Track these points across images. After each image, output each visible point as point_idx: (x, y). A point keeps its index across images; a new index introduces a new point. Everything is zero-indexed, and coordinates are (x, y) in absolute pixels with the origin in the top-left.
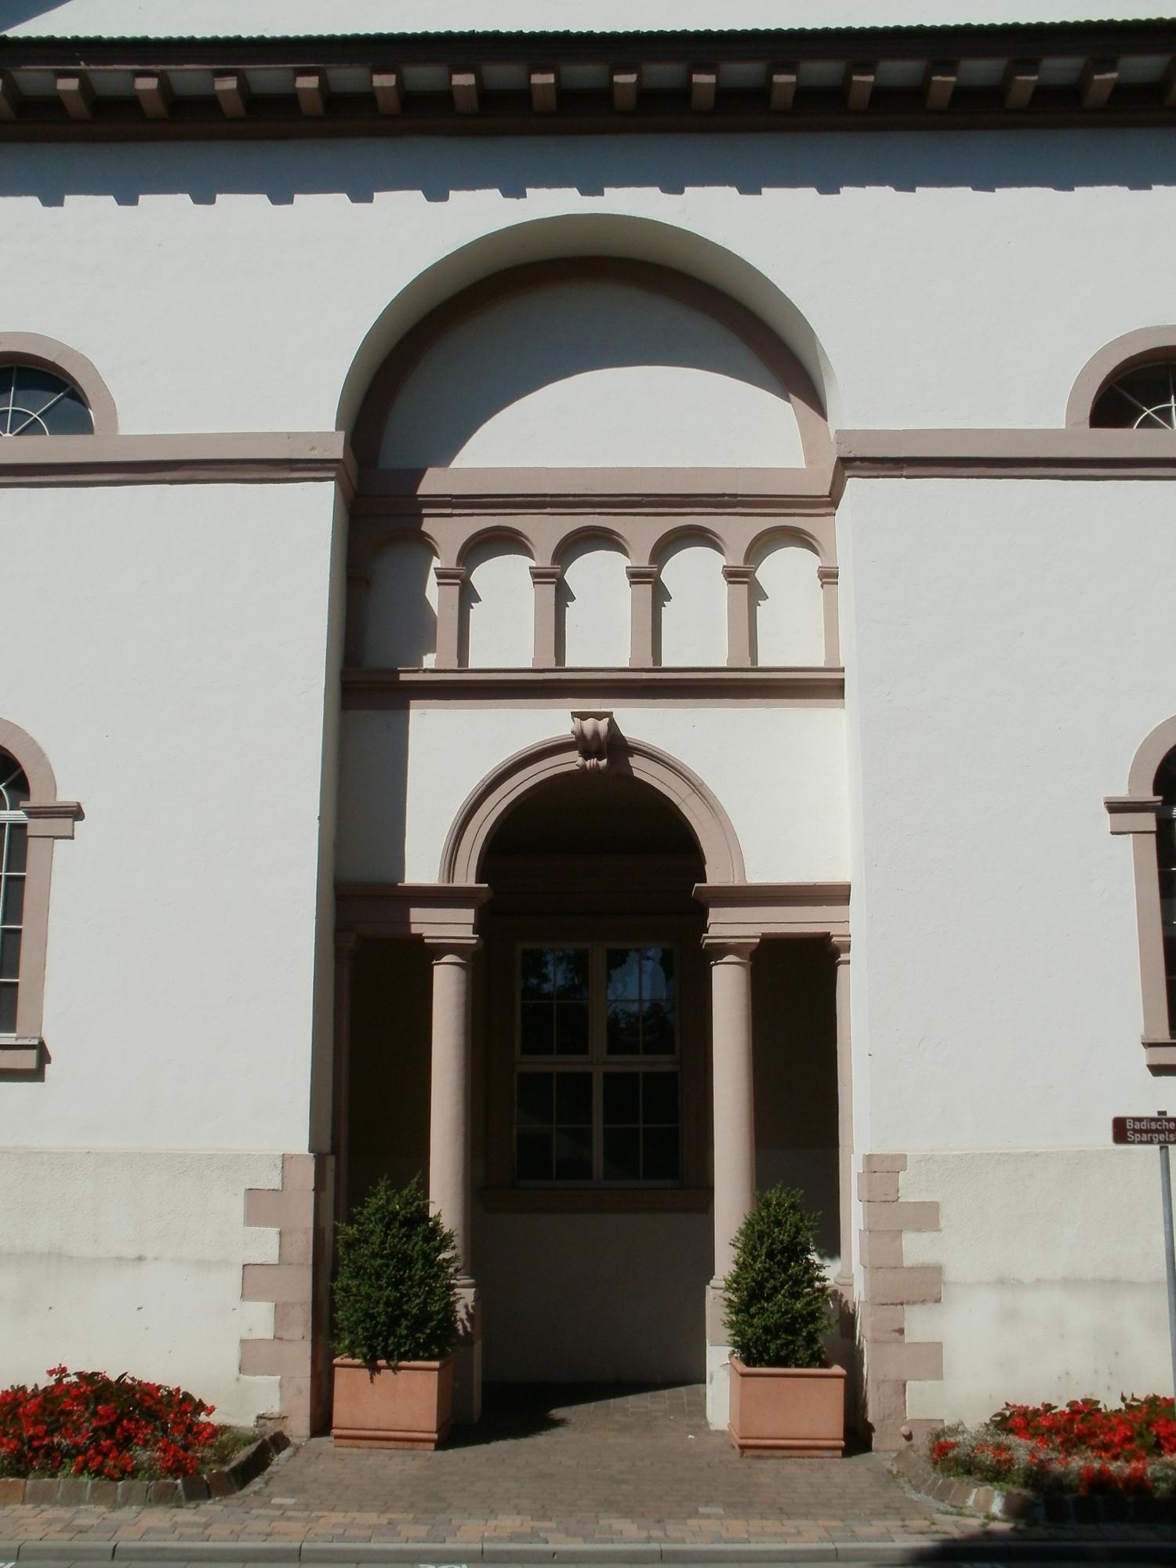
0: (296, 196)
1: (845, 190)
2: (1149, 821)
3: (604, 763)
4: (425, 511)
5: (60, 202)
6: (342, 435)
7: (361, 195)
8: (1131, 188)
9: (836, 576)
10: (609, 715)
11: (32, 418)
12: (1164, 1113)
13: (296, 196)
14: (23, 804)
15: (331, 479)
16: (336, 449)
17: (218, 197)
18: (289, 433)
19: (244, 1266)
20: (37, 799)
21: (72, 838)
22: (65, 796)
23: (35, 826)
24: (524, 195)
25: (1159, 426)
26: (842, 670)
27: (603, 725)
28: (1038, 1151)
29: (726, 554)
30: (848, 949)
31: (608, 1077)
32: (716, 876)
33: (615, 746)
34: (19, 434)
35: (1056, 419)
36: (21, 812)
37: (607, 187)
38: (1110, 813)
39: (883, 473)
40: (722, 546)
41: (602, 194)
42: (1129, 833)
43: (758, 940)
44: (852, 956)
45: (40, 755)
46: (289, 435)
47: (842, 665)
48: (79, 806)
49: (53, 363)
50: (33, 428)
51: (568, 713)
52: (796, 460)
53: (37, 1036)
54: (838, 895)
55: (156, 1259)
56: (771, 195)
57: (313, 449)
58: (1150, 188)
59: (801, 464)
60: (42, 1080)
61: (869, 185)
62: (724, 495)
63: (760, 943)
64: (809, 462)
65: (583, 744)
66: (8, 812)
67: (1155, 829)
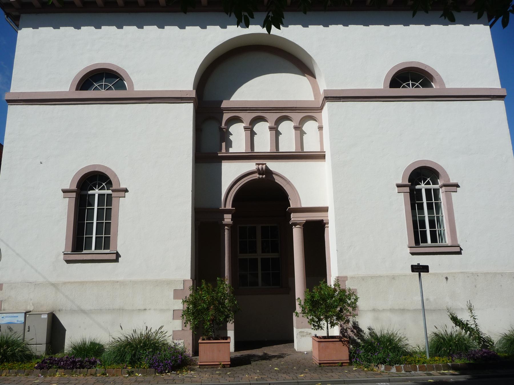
0: (124, 27)
1: (449, 25)
2: (407, 189)
3: (264, 176)
4: (224, 112)
5: (163, 28)
6: (195, 91)
7: (204, 27)
8: (404, 26)
9: (322, 128)
10: (265, 164)
11: (110, 86)
12: (419, 264)
13: (124, 27)
14: (110, 188)
15: (192, 103)
16: (194, 95)
17: (102, 27)
18: (181, 90)
19: (173, 310)
20: (114, 187)
21: (125, 197)
22: (123, 186)
23: (114, 194)
24: (328, 27)
25: (99, 90)
26: (325, 152)
27: (264, 166)
28: (382, 275)
29: (269, 122)
30: (328, 223)
31: (262, 259)
32: (292, 206)
33: (268, 172)
34: (107, 90)
35: (381, 87)
36: (110, 191)
37: (61, 27)
38: (63, 193)
39: (336, 101)
40: (292, 119)
41: (328, 27)
42: (402, 192)
43: (305, 222)
44: (329, 225)
45: (115, 175)
46: (181, 91)
47: (325, 151)
48: (126, 189)
49: (115, 71)
50: (110, 88)
51: (255, 164)
52: (312, 98)
53: (116, 250)
54: (325, 210)
55: (149, 309)
56: (333, 28)
57: (187, 95)
58: (59, 28)
59: (313, 99)
60: (118, 262)
61: (333, 25)
62: (293, 107)
63: (305, 223)
64: (315, 99)
65: (259, 172)
66: (106, 191)
67: (409, 191)
